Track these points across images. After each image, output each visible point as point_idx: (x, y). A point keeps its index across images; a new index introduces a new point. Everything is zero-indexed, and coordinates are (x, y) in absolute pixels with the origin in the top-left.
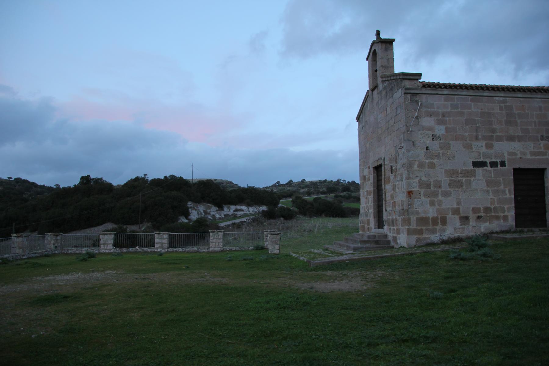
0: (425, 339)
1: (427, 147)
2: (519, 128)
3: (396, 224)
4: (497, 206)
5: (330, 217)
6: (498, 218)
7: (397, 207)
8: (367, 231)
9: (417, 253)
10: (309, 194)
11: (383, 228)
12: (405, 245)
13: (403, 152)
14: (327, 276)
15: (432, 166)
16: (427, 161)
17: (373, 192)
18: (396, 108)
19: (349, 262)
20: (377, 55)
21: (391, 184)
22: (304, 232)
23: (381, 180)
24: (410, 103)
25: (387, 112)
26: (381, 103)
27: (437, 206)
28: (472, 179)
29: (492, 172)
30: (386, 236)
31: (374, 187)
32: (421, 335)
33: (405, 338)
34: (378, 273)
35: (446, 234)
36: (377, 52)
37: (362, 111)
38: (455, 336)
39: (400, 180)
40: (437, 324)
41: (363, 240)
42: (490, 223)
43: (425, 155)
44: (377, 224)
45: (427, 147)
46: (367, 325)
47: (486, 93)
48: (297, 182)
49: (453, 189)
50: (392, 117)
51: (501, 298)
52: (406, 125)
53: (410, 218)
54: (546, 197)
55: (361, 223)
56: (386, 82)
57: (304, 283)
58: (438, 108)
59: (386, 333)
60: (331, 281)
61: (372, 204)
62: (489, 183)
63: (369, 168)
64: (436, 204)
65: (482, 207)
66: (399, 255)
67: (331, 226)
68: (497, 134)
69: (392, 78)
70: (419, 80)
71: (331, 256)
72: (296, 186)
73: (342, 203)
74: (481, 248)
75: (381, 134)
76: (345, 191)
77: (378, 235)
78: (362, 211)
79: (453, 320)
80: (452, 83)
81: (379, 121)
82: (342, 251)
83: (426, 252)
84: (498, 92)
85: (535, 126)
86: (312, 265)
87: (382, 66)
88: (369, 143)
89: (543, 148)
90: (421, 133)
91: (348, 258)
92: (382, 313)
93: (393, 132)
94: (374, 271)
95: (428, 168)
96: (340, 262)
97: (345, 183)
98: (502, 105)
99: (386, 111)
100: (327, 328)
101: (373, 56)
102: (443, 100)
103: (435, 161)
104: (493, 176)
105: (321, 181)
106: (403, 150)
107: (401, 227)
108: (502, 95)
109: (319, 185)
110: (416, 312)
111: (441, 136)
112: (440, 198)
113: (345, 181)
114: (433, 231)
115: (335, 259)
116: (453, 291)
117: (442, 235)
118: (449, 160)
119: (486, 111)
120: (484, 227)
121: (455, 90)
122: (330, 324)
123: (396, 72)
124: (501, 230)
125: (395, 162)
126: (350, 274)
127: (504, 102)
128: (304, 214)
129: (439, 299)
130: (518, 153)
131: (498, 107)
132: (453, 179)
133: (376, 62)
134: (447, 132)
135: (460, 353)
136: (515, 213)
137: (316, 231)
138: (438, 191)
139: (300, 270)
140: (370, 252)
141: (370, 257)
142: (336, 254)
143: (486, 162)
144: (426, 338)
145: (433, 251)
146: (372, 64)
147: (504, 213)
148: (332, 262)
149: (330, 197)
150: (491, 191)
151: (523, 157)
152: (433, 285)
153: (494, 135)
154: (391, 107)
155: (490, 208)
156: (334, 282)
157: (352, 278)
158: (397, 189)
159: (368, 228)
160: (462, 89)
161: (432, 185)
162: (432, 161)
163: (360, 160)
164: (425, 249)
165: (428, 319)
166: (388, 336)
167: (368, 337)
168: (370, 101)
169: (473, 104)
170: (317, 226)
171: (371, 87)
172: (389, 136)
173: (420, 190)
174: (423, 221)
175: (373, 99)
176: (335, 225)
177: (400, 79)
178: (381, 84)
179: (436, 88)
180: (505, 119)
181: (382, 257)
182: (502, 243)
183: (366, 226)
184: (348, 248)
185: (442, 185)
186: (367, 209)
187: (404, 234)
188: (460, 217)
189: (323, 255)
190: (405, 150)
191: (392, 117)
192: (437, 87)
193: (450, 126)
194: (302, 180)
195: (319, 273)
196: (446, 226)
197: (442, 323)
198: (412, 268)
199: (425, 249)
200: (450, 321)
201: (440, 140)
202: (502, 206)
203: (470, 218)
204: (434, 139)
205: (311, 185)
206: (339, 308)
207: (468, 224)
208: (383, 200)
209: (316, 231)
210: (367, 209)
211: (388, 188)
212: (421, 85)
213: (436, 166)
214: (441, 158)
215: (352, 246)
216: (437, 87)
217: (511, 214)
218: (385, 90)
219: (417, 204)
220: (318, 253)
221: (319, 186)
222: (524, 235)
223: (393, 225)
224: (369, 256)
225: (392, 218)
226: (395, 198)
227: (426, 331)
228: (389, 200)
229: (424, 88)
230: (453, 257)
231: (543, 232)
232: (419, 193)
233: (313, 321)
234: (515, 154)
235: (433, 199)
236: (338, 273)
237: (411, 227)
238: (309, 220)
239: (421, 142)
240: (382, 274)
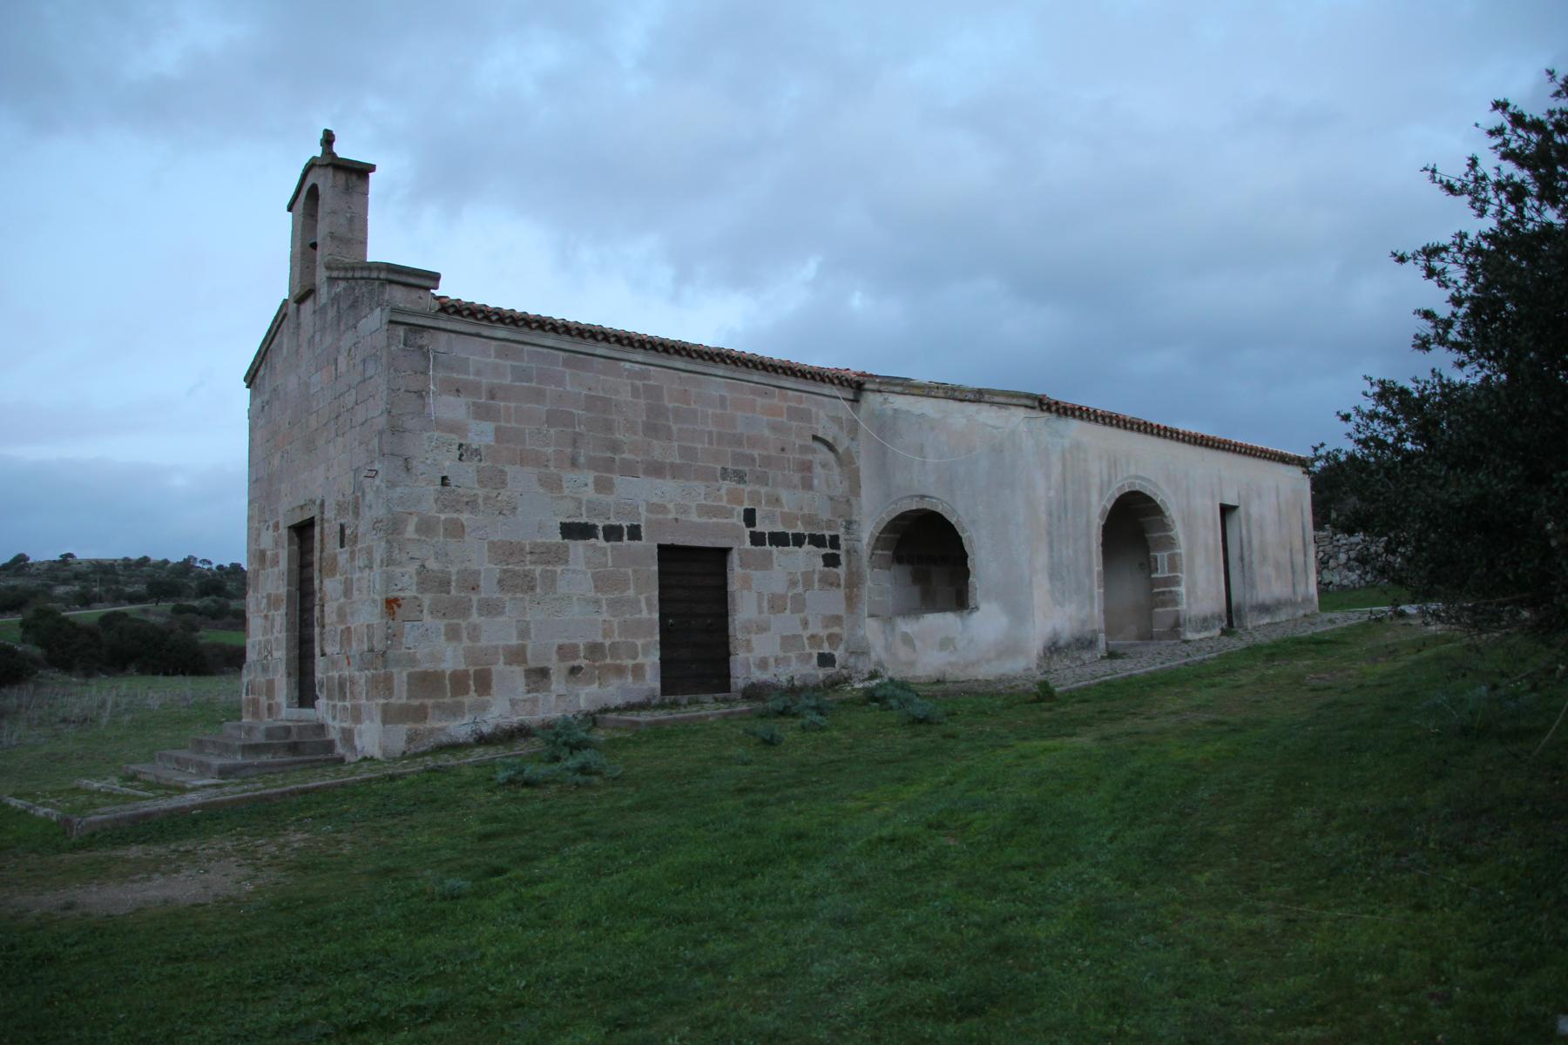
0: (414, 1015)
1: (444, 478)
2: (676, 444)
3: (352, 693)
4: (618, 639)
5: (155, 673)
6: (620, 671)
7: (354, 644)
8: (266, 716)
9: (409, 773)
10: (86, 600)
11: (313, 706)
12: (378, 754)
13: (378, 487)
14: (125, 861)
15: (456, 530)
16: (443, 517)
17: (285, 598)
18: (364, 361)
19: (201, 814)
20: (320, 202)
21: (338, 577)
22: (62, 726)
23: (311, 564)
24: (404, 350)
25: (336, 370)
26: (321, 340)
27: (466, 642)
28: (559, 569)
29: (609, 553)
30: (321, 728)
31: (289, 585)
32: (404, 1004)
33: (357, 1021)
34: (292, 839)
35: (490, 716)
36: (320, 192)
37: (263, 359)
38: (493, 995)
39: (366, 567)
40: (449, 968)
41: (252, 742)
42: (600, 684)
43: (436, 501)
44: (296, 694)
45: (444, 478)
46: (245, 1001)
47: (602, 349)
48: (43, 563)
49: (510, 595)
50: (349, 386)
51: (615, 877)
52: (389, 412)
53: (392, 674)
54: (730, 619)
55: (247, 690)
56: (340, 282)
57: (42, 894)
58: (478, 373)
59: (301, 1015)
60: (137, 877)
61: (283, 635)
62: (603, 581)
63: (276, 526)
64: (465, 635)
65: (581, 643)
66: (356, 780)
67: (158, 703)
68: (623, 456)
69: (358, 274)
70: (432, 291)
71: (143, 798)
72: (39, 574)
73: (198, 631)
74: (575, 752)
75: (317, 430)
76: (207, 594)
77: (299, 727)
78: (251, 655)
79: (493, 950)
80: (519, 310)
81: (312, 392)
82: (183, 779)
83: (433, 770)
84: (629, 349)
85: (711, 443)
86: (75, 833)
87: (332, 236)
88: (279, 454)
89: (725, 498)
90: (429, 438)
91: (200, 800)
92: (294, 957)
93: (351, 427)
94: (279, 835)
95: (445, 536)
96: (171, 814)
97: (209, 569)
98: (639, 383)
99: (334, 367)
100: (112, 1030)
101: (306, 200)
102: (492, 352)
103: (465, 517)
104: (610, 564)
105: (130, 560)
106: (377, 481)
107: (363, 701)
108: (639, 358)
109: (120, 572)
110: (393, 941)
111: (482, 449)
112: (475, 618)
113: (210, 563)
114: (455, 711)
115: (156, 808)
116: (499, 871)
117: (478, 720)
118: (501, 516)
119: (601, 394)
120: (587, 696)
121: (526, 330)
122: (121, 1016)
123: (370, 259)
124: (628, 703)
125: (354, 513)
126: (204, 849)
127: (644, 376)
128: (66, 666)
129: (458, 897)
130: (671, 506)
131: (629, 388)
132: (510, 567)
133: (316, 221)
134: (498, 439)
135: (504, 1038)
136: (660, 659)
137: (104, 721)
138: (470, 600)
139: (34, 851)
140: (271, 777)
141: (268, 795)
142: (162, 792)
143: (595, 527)
144: (418, 1010)
145: (453, 766)
146: (304, 225)
147: (635, 658)
148: (146, 815)
149: (157, 613)
150: (604, 602)
151: (682, 517)
152: (449, 860)
153: (617, 458)
154: (349, 354)
155: (602, 645)
156: (149, 879)
157: (210, 860)
158: (355, 593)
159: (270, 708)
160: (544, 330)
161: (453, 584)
162: (455, 515)
163: (250, 502)
164: (430, 761)
165: (424, 958)
166: (307, 1023)
167: (245, 1037)
168: (291, 330)
169: (568, 371)
170: (109, 704)
171: (297, 291)
172: (340, 439)
173: (419, 596)
174: (427, 682)
175: (298, 326)
176: (171, 700)
177: (378, 279)
178: (326, 285)
179: (476, 318)
180: (644, 418)
181: (306, 792)
182: (628, 735)
183: (263, 700)
184: (203, 768)
185: (482, 583)
186: (267, 649)
187: (372, 721)
188: (525, 671)
189: (118, 796)
190: (382, 481)
191: (349, 386)
192: (479, 316)
193: (508, 425)
194: (61, 556)
195: (101, 854)
197: (461, 964)
198: (394, 817)
199: (430, 761)
200: (483, 956)
201: (481, 460)
202: (629, 640)
203: (551, 671)
204: (463, 458)
205: (93, 572)
206: (157, 958)
207: (548, 689)
208: (316, 624)
209: (104, 721)
210: (267, 649)
211: (329, 588)
212: (437, 307)
213: (468, 530)
214: (482, 508)
215: (217, 762)
216: (479, 316)
217: (652, 660)
218: (335, 307)
219: (410, 635)
220: (102, 790)
221: (121, 578)
222: (679, 714)
223: (343, 697)
224: (267, 791)
225: (340, 677)
226: (349, 617)
227: (419, 992)
228: (331, 624)
229: (443, 315)
230: (505, 780)
231: (722, 705)
232: (418, 603)
233: (65, 1015)
234: (662, 509)
235: (455, 621)
236: (164, 850)
237: (392, 700)
238: (82, 685)
239: (429, 462)
240: (304, 840)
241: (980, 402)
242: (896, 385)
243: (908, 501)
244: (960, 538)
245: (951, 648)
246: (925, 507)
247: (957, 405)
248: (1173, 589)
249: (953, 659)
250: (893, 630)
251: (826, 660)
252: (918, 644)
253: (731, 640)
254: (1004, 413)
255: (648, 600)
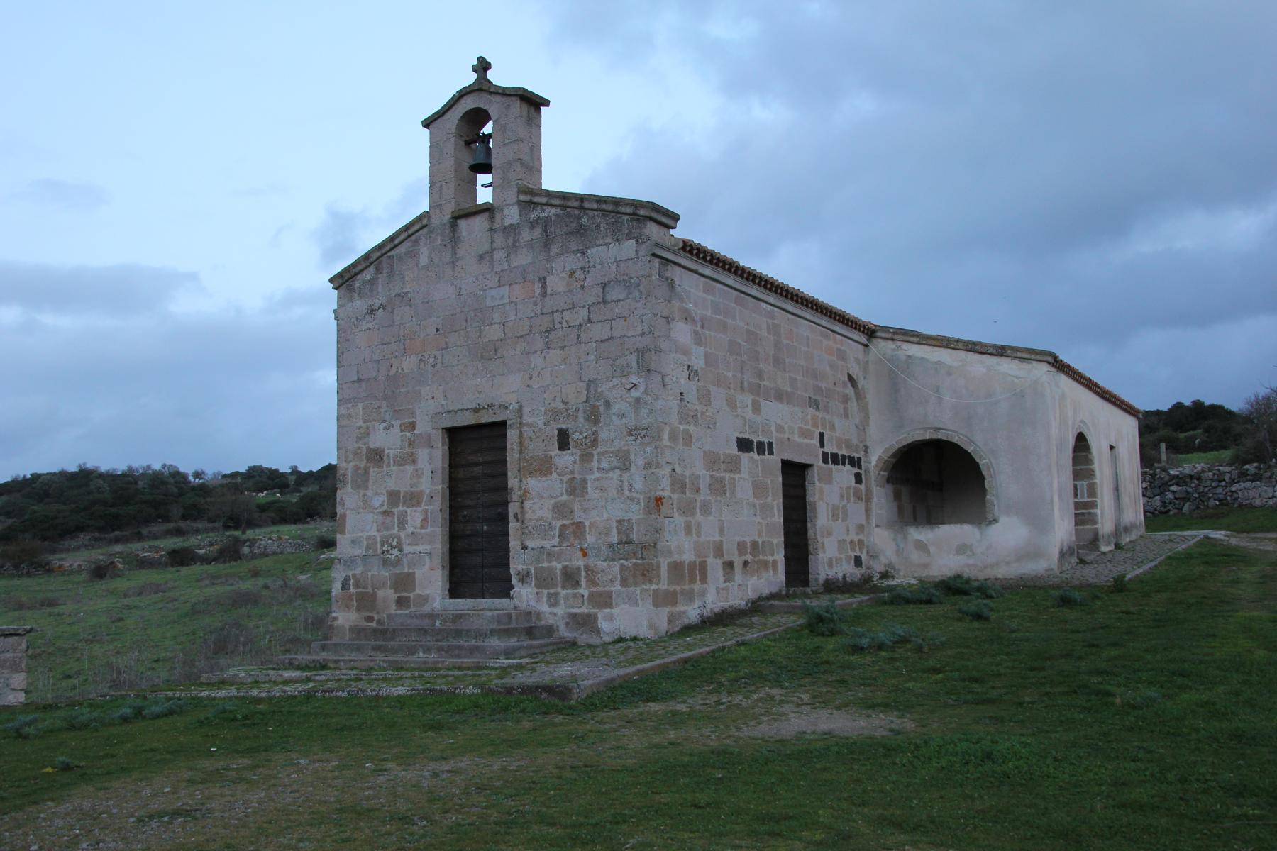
16: (682, 427)
28: (737, 476)
54: (809, 525)
161: (687, 486)
180: (773, 352)
185: (701, 487)
196: (706, 583)
241: (1002, 355)
242: (913, 336)
243: (922, 432)
244: (977, 465)
245: (969, 552)
246: (939, 437)
247: (977, 356)
248: (1092, 511)
249: (971, 561)
250: (905, 538)
251: (858, 562)
252: (932, 549)
253: (810, 542)
254: (1026, 366)
255: (778, 505)
